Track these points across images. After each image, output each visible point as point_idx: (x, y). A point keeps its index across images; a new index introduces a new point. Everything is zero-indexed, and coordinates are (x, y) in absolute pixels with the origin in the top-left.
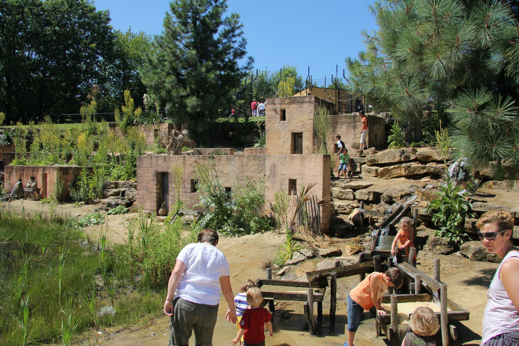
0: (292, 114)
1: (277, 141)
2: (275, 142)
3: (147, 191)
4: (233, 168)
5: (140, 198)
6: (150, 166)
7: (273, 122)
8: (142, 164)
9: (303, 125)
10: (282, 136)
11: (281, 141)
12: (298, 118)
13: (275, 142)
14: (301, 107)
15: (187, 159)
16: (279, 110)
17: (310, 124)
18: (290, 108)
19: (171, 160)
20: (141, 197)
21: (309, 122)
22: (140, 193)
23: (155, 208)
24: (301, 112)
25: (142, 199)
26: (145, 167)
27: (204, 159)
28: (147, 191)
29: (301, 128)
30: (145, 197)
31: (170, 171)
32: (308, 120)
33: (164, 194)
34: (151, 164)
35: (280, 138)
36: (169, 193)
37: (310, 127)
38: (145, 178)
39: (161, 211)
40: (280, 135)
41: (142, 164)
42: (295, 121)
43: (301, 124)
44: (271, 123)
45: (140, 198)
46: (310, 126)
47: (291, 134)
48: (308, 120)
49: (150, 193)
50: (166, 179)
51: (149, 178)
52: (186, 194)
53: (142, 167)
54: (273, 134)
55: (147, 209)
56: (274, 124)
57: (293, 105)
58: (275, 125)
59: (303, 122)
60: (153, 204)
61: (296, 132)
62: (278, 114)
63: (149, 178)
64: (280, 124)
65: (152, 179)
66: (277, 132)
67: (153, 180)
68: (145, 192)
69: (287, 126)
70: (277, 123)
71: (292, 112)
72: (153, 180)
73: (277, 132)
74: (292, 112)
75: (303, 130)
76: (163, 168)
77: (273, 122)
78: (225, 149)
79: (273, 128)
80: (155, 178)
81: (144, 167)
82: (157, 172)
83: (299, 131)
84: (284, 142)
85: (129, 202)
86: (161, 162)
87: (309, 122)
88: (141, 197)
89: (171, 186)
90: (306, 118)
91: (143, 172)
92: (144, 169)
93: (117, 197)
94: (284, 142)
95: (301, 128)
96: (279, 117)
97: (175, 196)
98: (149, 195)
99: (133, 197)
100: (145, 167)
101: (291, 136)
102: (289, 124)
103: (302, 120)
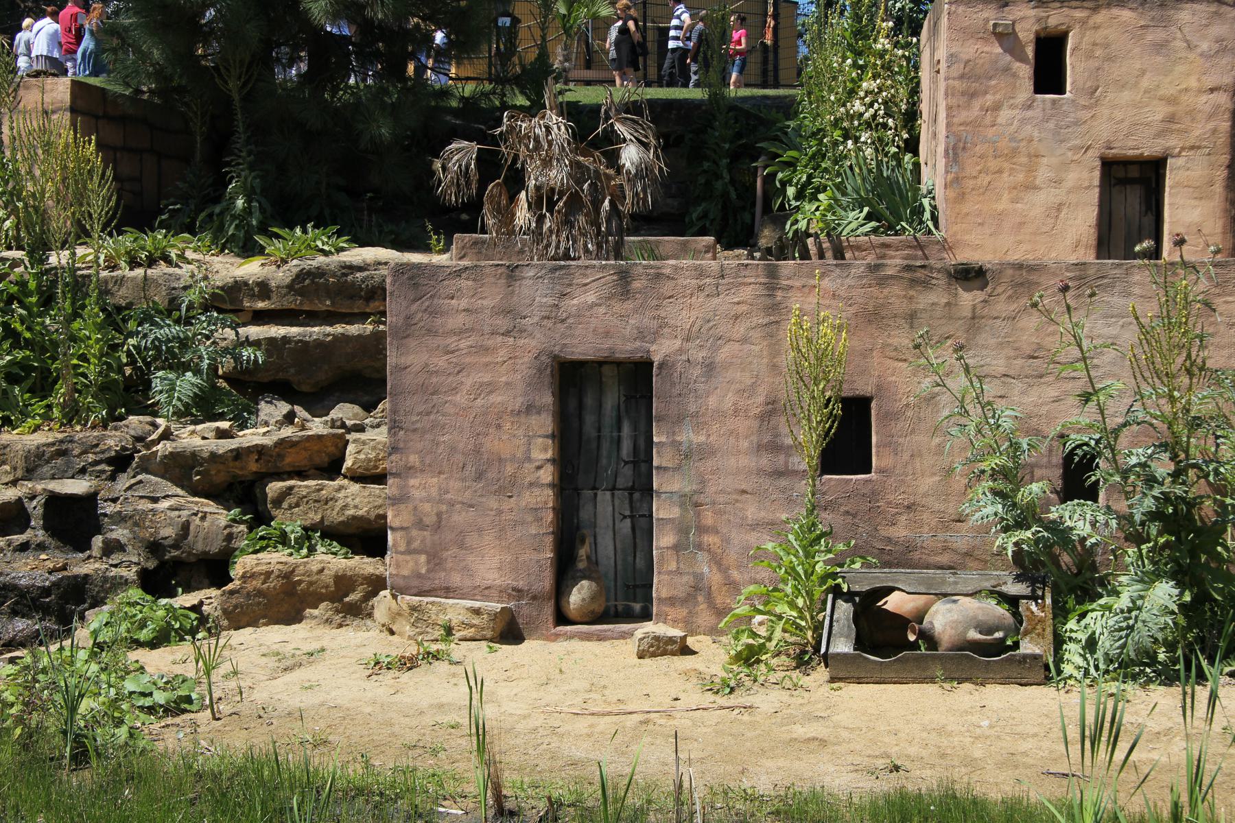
0: (1110, 59)
1: (1014, 201)
2: (1003, 204)
3: (479, 476)
4: (1113, 331)
5: (420, 524)
6: (503, 323)
7: (989, 99)
8: (433, 312)
9: (1171, 119)
10: (1043, 174)
11: (1041, 200)
12: (1145, 83)
13: (1003, 204)
14: (1165, 23)
15: (797, 283)
16: (1026, 35)
17: (1210, 117)
18: (1096, 28)
19: (667, 288)
20: (430, 520)
21: (1205, 102)
22: (417, 494)
23: (546, 582)
24: (1160, 47)
25: (438, 527)
26: (461, 332)
27: (914, 282)
28: (479, 476)
29: (1159, 134)
30: (459, 518)
31: (659, 352)
32: (1200, 91)
33: (577, 490)
34: (507, 311)
35: (1031, 187)
36: (1061, 461)
37: (1214, 131)
38: (460, 398)
39: (579, 595)
40: (1031, 170)
41: (433, 312)
42: (1126, 96)
43: (1158, 112)
44: (977, 104)
45: (420, 524)
46: (1210, 125)
47: (1098, 163)
48: (1200, 91)
49: (500, 491)
50: (589, 401)
51: (497, 398)
52: (783, 482)
53: (431, 332)
54: (993, 164)
55: (484, 592)
56: (997, 107)
57: (1115, 11)
58: (1005, 115)
59: (1172, 101)
60: (529, 556)
61: (1131, 153)
62: (1022, 59)
63: (497, 398)
64: (1036, 113)
65: (519, 403)
66: (1015, 152)
67: (529, 409)
68: (455, 485)
69: (1076, 123)
70: (1012, 107)
71: (1107, 46)
72: (529, 409)
73: (1015, 152)
74: (1107, 46)
75: (1173, 142)
76: (607, 334)
77: (989, 99)
78: (685, 244)
79: (990, 132)
80: (548, 399)
81: (453, 332)
82: (556, 358)
83: (1149, 148)
84: (1059, 207)
85: (151, 565)
86: (591, 298)
87: (1205, 102)
88: (430, 520)
89: (676, 445)
90: (1193, 83)
91: (441, 362)
92: (452, 341)
93: (19, 539)
94: (1059, 207)
95: (1159, 134)
96: (1025, 72)
97: (702, 498)
98: (493, 503)
99: (186, 527)
100: (461, 332)
101: (1097, 174)
102: (1085, 115)
103: (1171, 91)
